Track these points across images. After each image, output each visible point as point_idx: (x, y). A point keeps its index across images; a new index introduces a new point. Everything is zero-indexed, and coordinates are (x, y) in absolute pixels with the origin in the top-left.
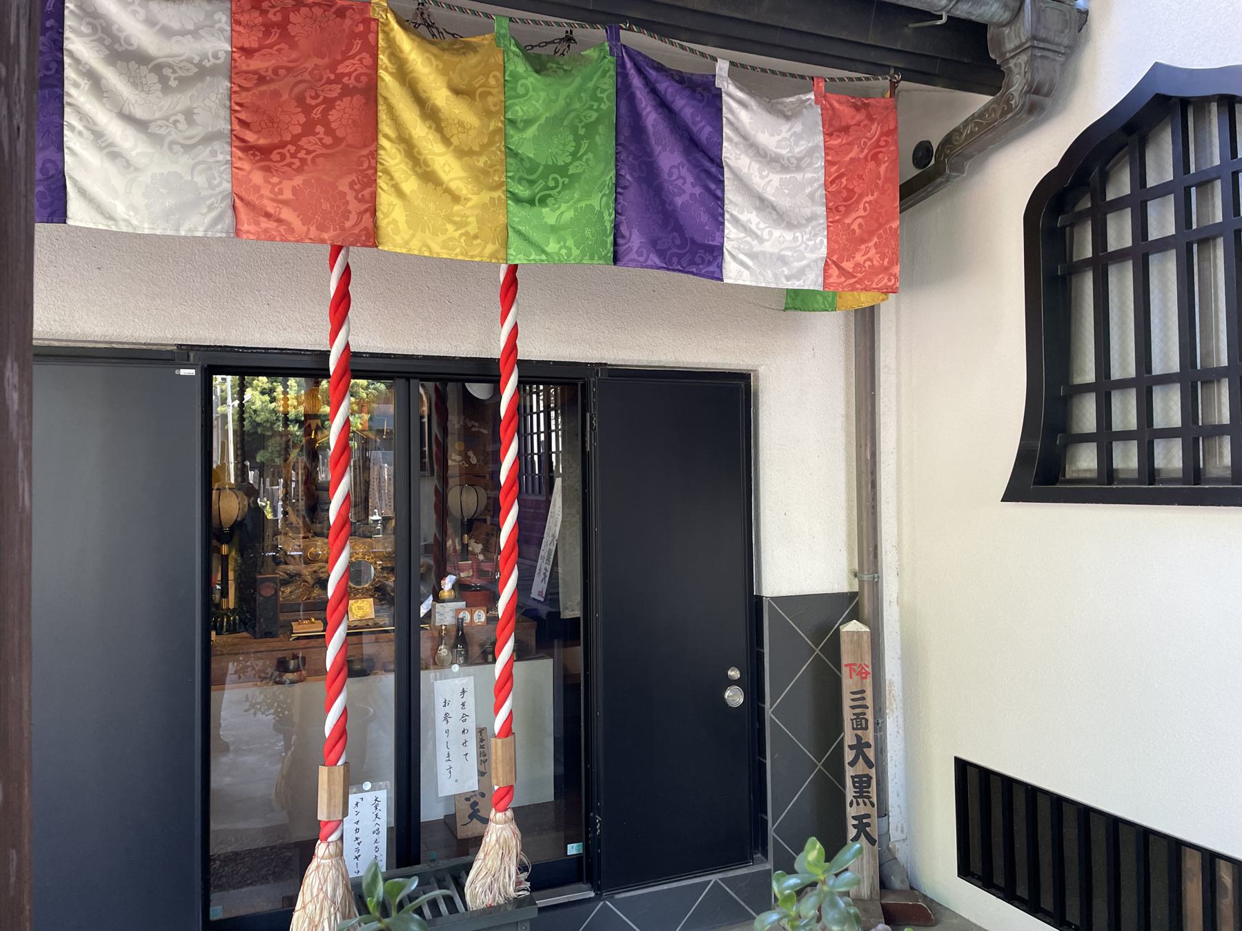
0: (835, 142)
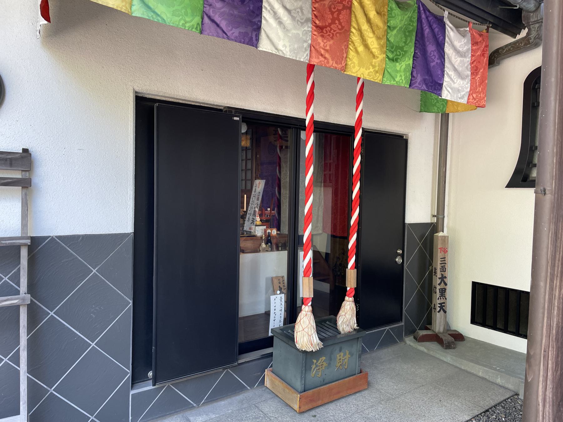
0: (474, 48)
